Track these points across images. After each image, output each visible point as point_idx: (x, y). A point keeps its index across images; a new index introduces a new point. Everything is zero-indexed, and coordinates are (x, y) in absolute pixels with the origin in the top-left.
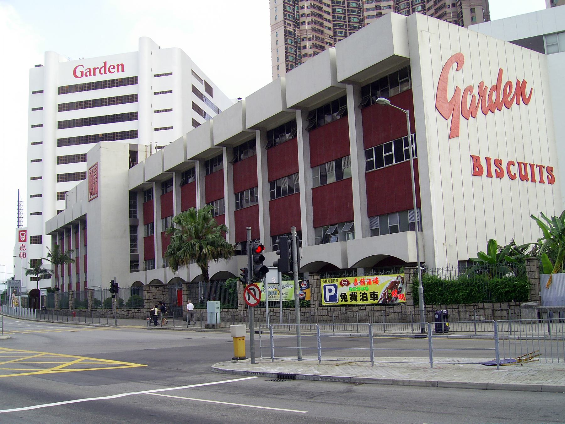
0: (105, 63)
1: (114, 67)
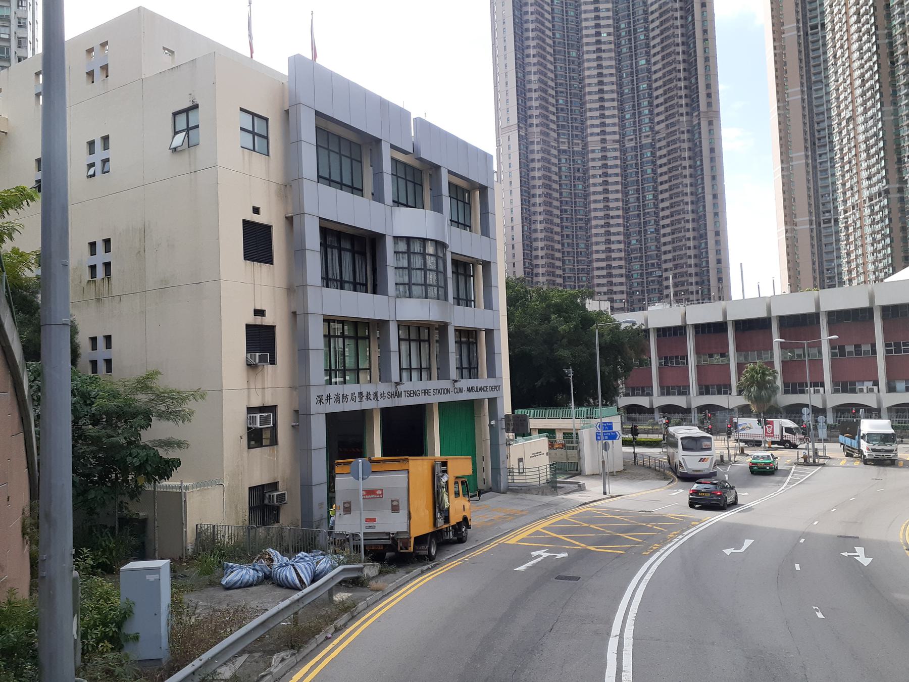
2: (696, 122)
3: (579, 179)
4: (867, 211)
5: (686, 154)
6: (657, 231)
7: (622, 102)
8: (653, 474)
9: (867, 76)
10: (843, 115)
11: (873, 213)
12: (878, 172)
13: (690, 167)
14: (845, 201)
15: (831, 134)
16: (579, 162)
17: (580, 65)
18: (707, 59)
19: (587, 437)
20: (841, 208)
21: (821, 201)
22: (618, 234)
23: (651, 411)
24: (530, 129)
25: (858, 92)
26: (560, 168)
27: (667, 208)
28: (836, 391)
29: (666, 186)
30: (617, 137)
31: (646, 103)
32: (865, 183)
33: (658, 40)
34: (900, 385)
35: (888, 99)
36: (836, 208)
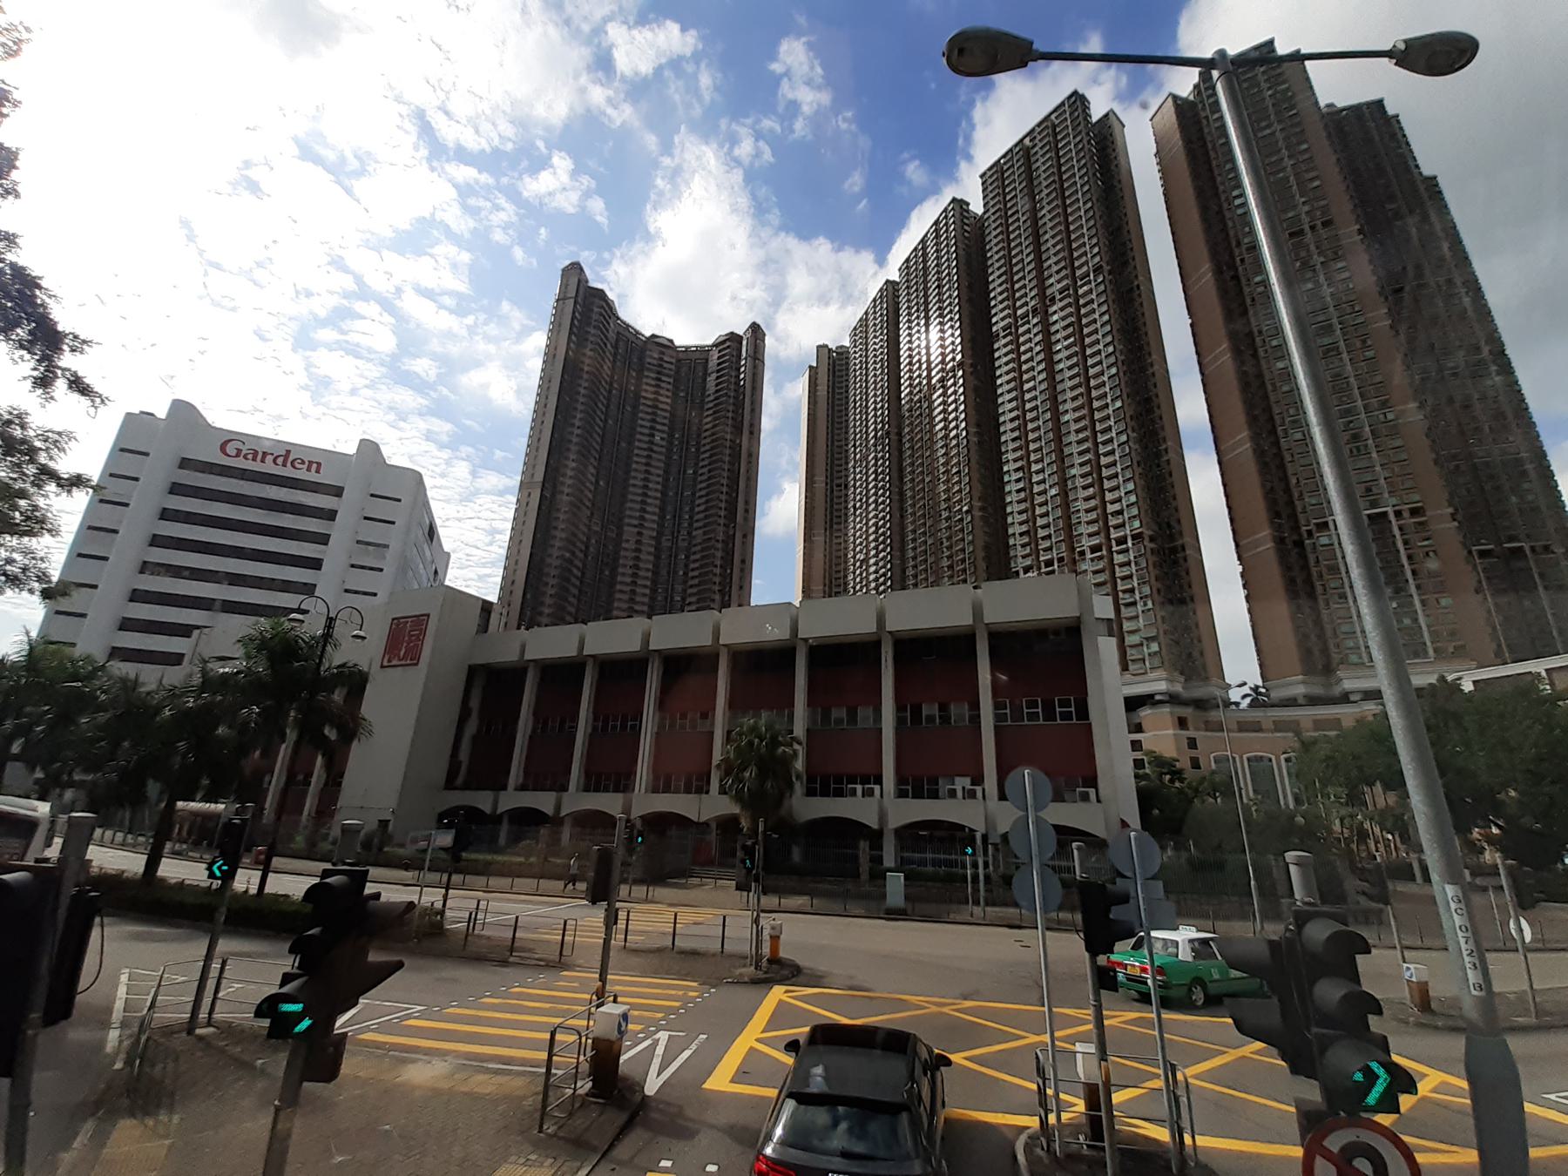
0: (288, 452)
1: (303, 462)
23: (556, 821)
28: (902, 794)
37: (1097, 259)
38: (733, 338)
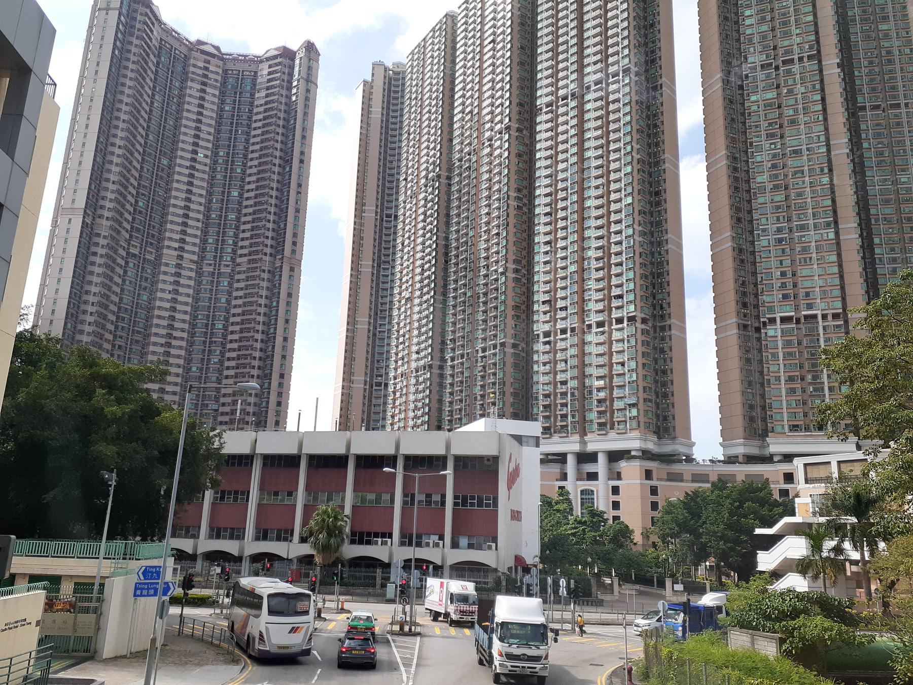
2: (278, 264)
3: (145, 289)
4: (413, 381)
5: (264, 293)
6: (221, 362)
7: (207, 225)
8: (211, 653)
9: (426, 266)
10: (403, 294)
11: (417, 383)
12: (426, 349)
13: (266, 306)
14: (396, 369)
15: (391, 309)
16: (149, 271)
17: (169, 175)
18: (297, 211)
19: (118, 590)
20: (392, 374)
21: (376, 365)
22: (179, 357)
24: (98, 220)
25: (418, 278)
26: (125, 272)
27: (236, 341)
28: (402, 544)
29: (238, 319)
30: (195, 258)
31: (231, 234)
32: (414, 356)
33: (254, 178)
34: (464, 541)
35: (440, 290)
36: (387, 374)
37: (627, 60)
38: (287, 54)
